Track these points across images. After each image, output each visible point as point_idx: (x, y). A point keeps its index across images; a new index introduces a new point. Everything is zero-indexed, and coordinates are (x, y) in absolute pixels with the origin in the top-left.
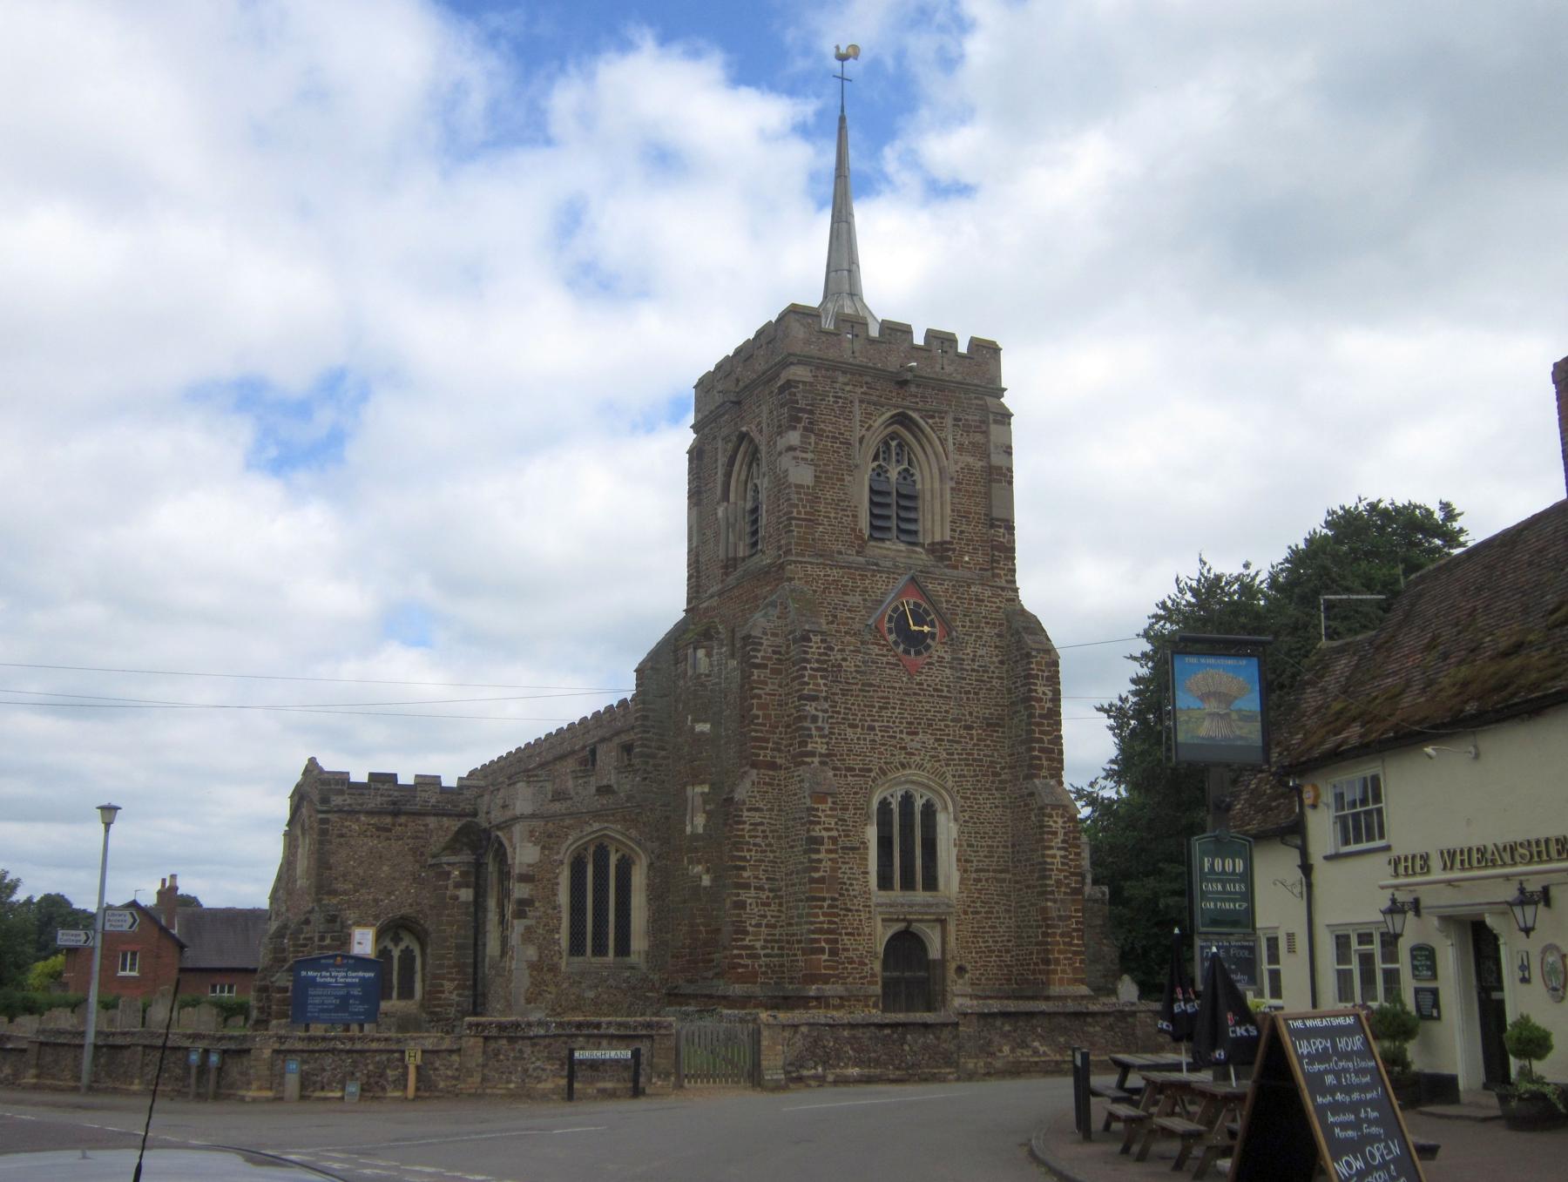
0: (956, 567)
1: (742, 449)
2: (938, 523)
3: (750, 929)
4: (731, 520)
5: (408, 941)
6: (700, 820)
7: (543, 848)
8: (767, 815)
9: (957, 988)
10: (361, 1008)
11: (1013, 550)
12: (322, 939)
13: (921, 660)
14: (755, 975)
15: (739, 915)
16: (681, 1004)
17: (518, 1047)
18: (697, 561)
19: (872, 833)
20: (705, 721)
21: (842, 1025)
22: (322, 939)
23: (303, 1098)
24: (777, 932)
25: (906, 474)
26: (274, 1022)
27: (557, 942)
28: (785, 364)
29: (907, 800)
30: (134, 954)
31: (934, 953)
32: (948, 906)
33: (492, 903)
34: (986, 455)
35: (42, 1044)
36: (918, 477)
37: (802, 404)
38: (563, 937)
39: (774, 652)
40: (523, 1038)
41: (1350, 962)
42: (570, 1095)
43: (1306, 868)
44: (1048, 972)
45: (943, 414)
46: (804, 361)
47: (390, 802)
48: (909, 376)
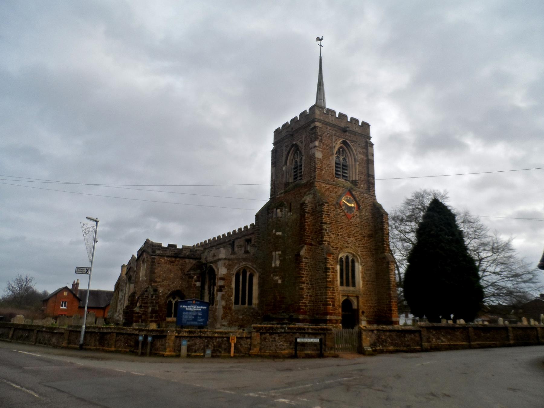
1: (292, 149)
2: (354, 174)
6: (278, 263)
7: (228, 269)
12: (152, 297)
17: (273, 336)
18: (274, 184)
22: (152, 297)
23: (188, 356)
25: (344, 159)
26: (134, 324)
27: (231, 300)
30: (65, 302)
31: (355, 307)
33: (206, 287)
35: (71, 331)
36: (347, 160)
38: (233, 298)
40: (275, 333)
42: (294, 356)
46: (319, 121)
47: (174, 254)
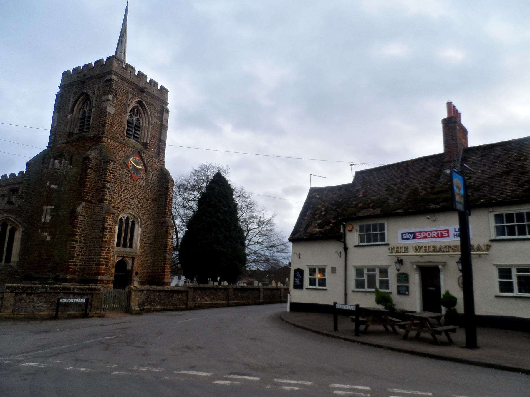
0: (149, 151)
1: (82, 97)
6: (48, 218)
8: (86, 218)
9: (135, 279)
17: (31, 297)
19: (117, 228)
20: (55, 185)
24: (84, 257)
29: (128, 219)
31: (129, 268)
36: (141, 122)
37: (114, 87)
39: (96, 165)
40: (34, 293)
41: (363, 277)
43: (346, 249)
46: (116, 74)
48: (146, 90)
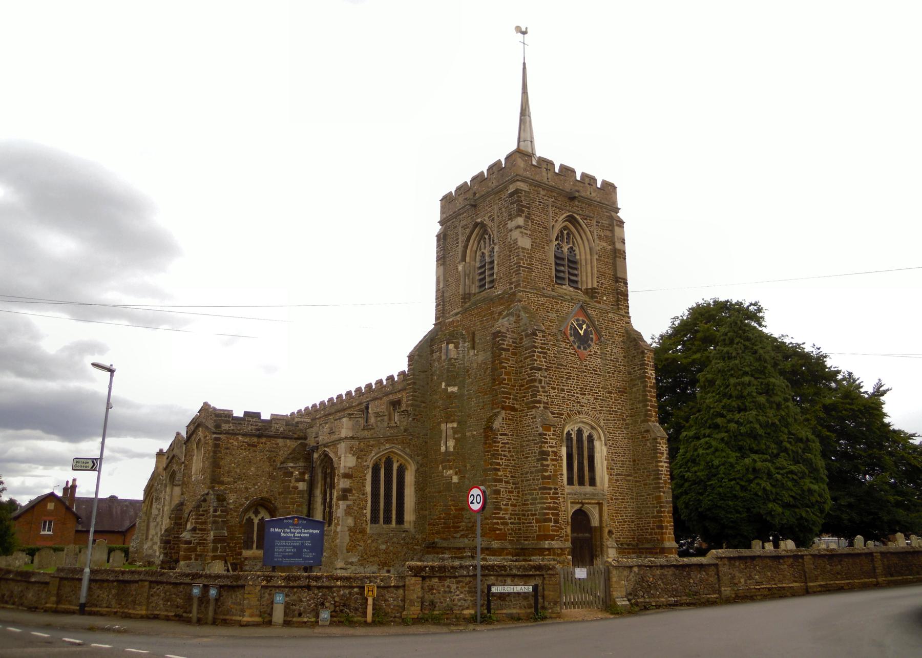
2: (589, 277)
3: (503, 507)
4: (467, 272)
5: (264, 515)
6: (451, 444)
7: (358, 458)
10: (311, 555)
11: (627, 296)
13: (586, 353)
14: (505, 535)
15: (497, 498)
16: (438, 553)
17: (446, 583)
19: (564, 451)
21: (656, 566)
22: (215, 511)
23: (287, 623)
24: (517, 509)
25: (571, 249)
28: (513, 181)
29: (580, 432)
30: (50, 522)
31: (595, 522)
32: (604, 495)
33: (318, 493)
34: (613, 243)
35: (62, 579)
36: (577, 252)
37: (524, 203)
38: (368, 512)
39: (513, 342)
44: (663, 534)
45: (591, 218)
